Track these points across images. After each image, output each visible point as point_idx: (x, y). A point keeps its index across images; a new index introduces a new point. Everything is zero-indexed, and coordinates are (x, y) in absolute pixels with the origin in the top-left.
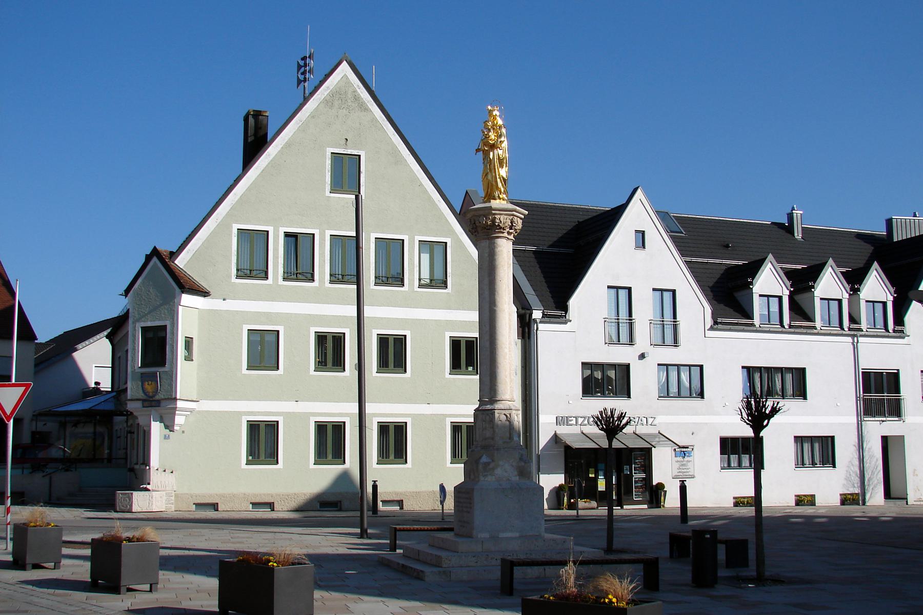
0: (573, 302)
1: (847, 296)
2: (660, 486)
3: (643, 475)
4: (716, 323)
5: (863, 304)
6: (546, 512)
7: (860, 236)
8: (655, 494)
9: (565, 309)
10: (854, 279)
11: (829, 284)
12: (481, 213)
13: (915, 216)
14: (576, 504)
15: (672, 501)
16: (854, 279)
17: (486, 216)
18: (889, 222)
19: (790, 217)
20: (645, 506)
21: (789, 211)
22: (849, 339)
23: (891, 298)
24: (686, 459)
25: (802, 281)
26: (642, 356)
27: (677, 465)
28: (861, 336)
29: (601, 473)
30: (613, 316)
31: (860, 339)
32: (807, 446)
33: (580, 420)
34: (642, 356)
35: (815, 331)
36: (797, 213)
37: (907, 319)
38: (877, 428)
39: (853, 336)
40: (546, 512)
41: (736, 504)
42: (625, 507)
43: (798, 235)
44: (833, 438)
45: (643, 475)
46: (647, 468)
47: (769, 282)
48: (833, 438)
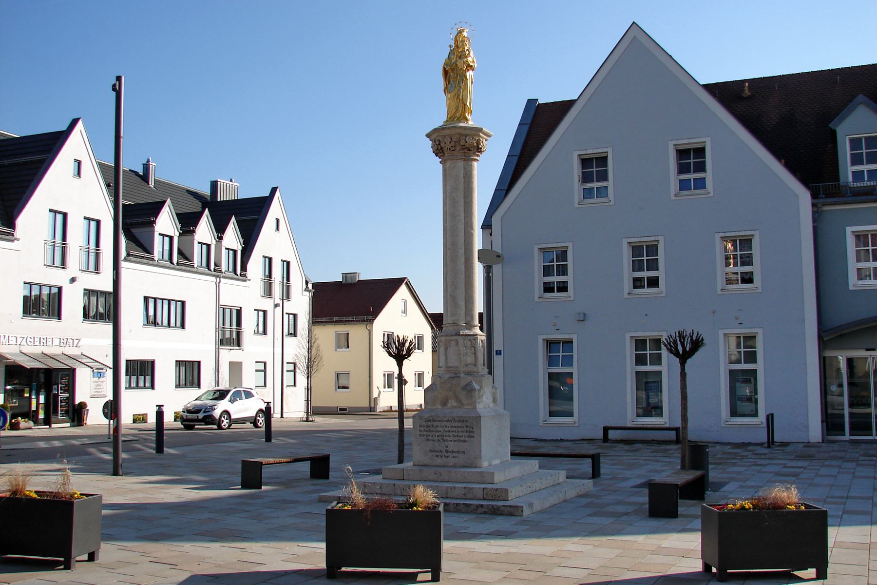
0: (20, 221)
1: (214, 242)
2: (83, 405)
3: (67, 395)
4: (128, 255)
5: (224, 252)
6: (849, 230)
7: (189, 192)
8: (77, 414)
9: (12, 225)
10: (220, 229)
11: (204, 231)
12: (468, 132)
13: (231, 181)
14: (18, 423)
15: (95, 418)
16: (220, 229)
17: (473, 136)
18: (214, 185)
19: (146, 167)
20: (68, 425)
21: (145, 162)
22: (214, 279)
23: (240, 248)
24: (102, 379)
25: (188, 222)
26: (73, 280)
27: (94, 385)
28: (224, 277)
29: (34, 392)
30: (50, 239)
31: (222, 280)
32: (183, 369)
33: (19, 340)
34: (73, 280)
35: (192, 269)
36: (153, 164)
37: (249, 266)
38: (229, 355)
39: (217, 276)
40: (849, 230)
41: (135, 421)
42: (53, 426)
43: (152, 184)
44: (199, 363)
45: (67, 395)
46: (71, 388)
47: (166, 223)
48: (199, 363)
